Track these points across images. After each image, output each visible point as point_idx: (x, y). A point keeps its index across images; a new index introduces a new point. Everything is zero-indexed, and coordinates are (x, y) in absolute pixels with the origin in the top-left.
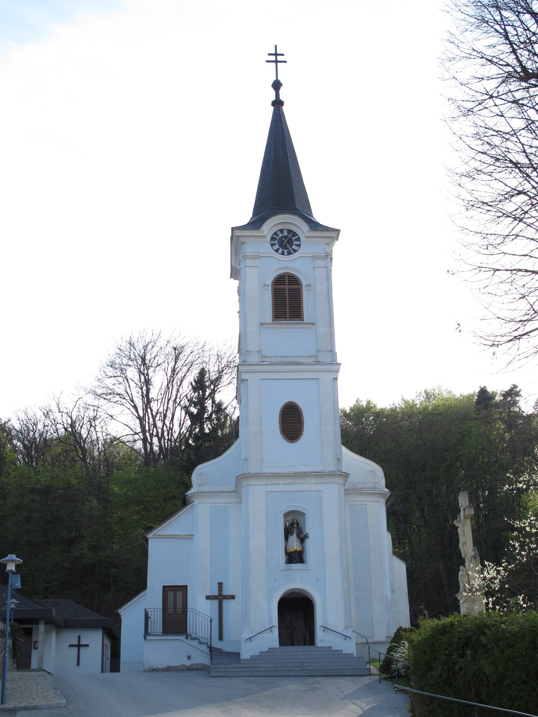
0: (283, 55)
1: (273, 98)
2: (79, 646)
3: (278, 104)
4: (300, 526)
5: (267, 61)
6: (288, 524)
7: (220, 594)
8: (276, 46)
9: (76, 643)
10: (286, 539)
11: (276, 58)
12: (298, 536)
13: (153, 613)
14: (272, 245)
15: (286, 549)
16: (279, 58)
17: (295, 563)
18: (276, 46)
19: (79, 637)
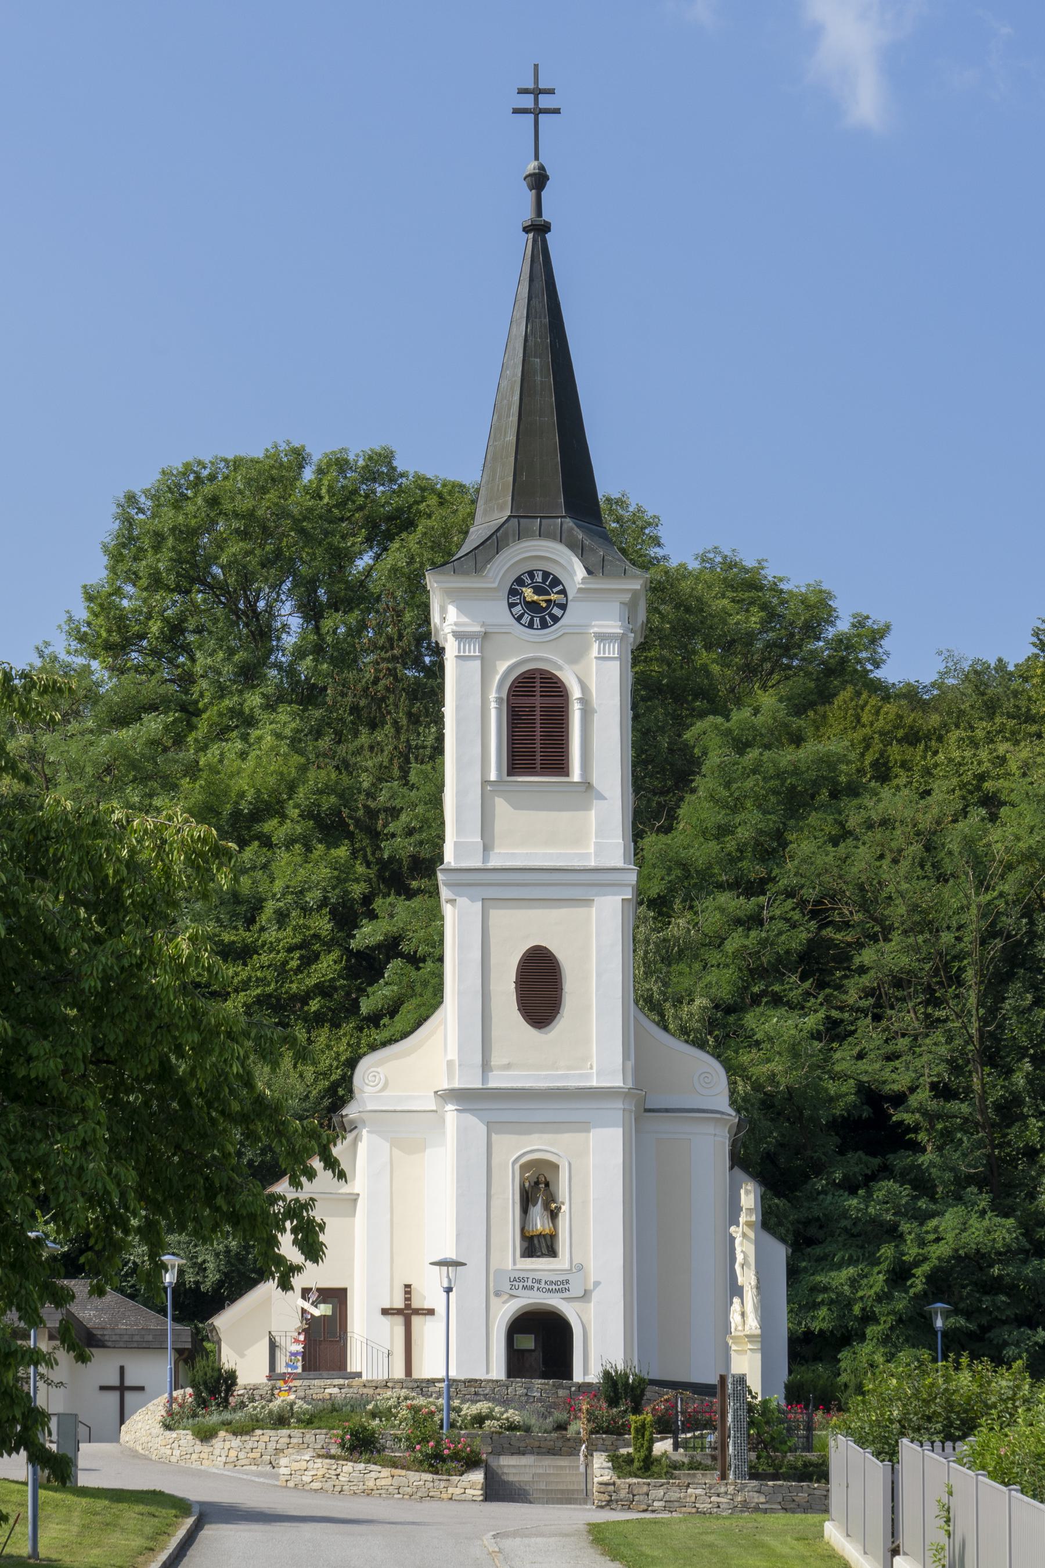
0: (551, 92)
1: (527, 215)
2: (122, 1389)
3: (539, 229)
4: (551, 1187)
5: (516, 111)
6: (527, 1184)
7: (408, 1306)
8: (536, 66)
9: (116, 1382)
10: (525, 1210)
11: (536, 103)
12: (546, 1206)
13: (283, 1339)
14: (511, 606)
15: (522, 1230)
16: (545, 102)
17: (538, 1257)
18: (536, 66)
19: (122, 1368)
